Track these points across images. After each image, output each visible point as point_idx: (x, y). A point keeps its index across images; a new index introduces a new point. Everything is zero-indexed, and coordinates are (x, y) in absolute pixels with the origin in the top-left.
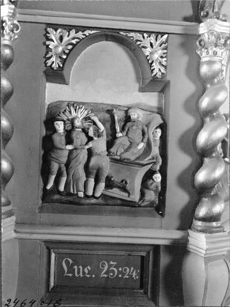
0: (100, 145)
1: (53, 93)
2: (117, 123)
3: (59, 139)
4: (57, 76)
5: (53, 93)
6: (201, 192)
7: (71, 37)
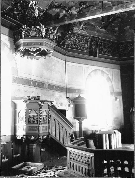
0: (33, 118)
1: (29, 114)
2: (34, 116)
3: (30, 118)
4: (30, 113)
5: (29, 114)
6: (41, 122)
7: (31, 110)
